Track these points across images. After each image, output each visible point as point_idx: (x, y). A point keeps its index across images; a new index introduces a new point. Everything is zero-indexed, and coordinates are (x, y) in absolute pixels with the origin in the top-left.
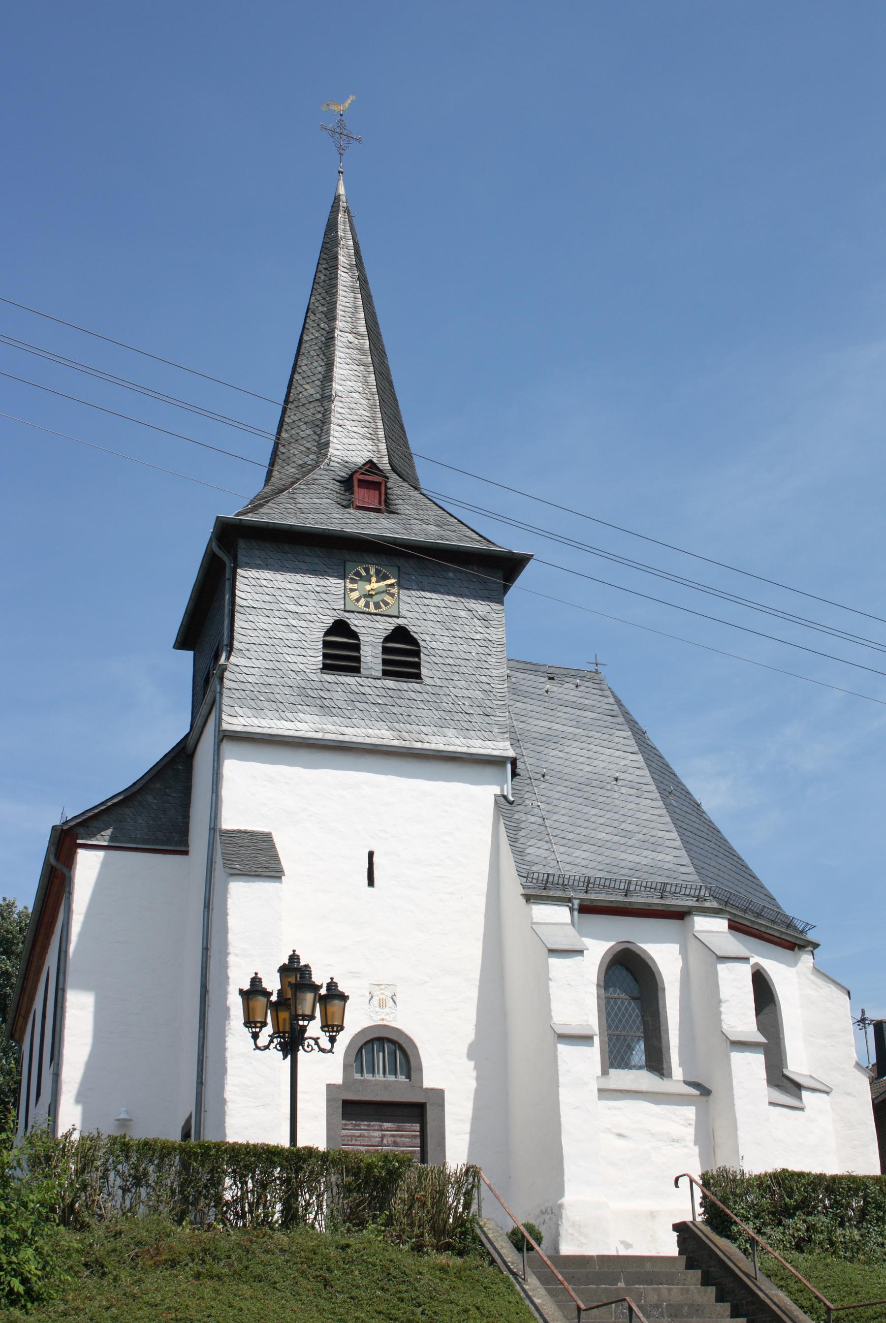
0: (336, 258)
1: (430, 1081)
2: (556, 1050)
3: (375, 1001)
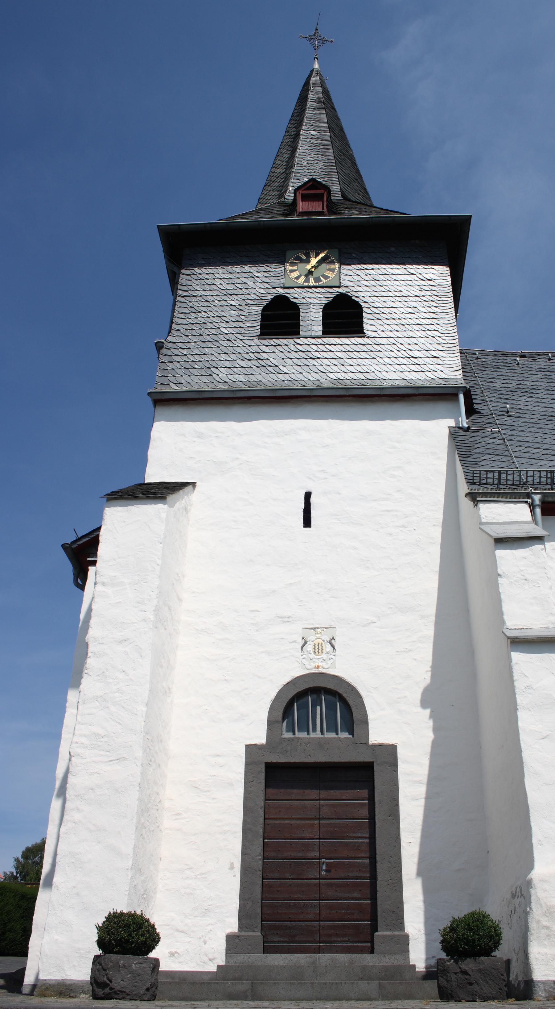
0: (307, 96)
1: (376, 736)
2: (510, 659)
3: (309, 647)
